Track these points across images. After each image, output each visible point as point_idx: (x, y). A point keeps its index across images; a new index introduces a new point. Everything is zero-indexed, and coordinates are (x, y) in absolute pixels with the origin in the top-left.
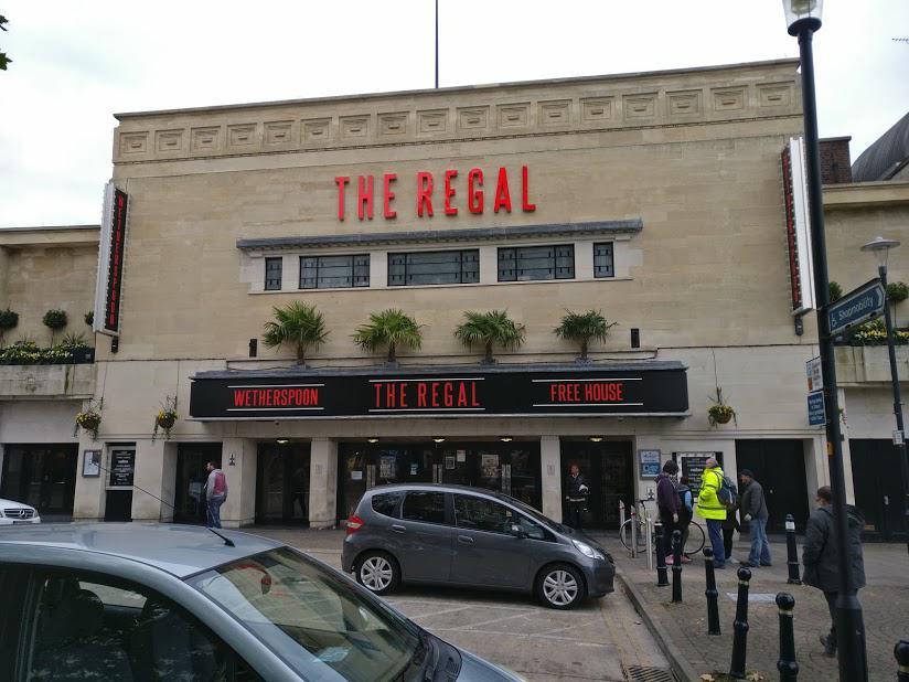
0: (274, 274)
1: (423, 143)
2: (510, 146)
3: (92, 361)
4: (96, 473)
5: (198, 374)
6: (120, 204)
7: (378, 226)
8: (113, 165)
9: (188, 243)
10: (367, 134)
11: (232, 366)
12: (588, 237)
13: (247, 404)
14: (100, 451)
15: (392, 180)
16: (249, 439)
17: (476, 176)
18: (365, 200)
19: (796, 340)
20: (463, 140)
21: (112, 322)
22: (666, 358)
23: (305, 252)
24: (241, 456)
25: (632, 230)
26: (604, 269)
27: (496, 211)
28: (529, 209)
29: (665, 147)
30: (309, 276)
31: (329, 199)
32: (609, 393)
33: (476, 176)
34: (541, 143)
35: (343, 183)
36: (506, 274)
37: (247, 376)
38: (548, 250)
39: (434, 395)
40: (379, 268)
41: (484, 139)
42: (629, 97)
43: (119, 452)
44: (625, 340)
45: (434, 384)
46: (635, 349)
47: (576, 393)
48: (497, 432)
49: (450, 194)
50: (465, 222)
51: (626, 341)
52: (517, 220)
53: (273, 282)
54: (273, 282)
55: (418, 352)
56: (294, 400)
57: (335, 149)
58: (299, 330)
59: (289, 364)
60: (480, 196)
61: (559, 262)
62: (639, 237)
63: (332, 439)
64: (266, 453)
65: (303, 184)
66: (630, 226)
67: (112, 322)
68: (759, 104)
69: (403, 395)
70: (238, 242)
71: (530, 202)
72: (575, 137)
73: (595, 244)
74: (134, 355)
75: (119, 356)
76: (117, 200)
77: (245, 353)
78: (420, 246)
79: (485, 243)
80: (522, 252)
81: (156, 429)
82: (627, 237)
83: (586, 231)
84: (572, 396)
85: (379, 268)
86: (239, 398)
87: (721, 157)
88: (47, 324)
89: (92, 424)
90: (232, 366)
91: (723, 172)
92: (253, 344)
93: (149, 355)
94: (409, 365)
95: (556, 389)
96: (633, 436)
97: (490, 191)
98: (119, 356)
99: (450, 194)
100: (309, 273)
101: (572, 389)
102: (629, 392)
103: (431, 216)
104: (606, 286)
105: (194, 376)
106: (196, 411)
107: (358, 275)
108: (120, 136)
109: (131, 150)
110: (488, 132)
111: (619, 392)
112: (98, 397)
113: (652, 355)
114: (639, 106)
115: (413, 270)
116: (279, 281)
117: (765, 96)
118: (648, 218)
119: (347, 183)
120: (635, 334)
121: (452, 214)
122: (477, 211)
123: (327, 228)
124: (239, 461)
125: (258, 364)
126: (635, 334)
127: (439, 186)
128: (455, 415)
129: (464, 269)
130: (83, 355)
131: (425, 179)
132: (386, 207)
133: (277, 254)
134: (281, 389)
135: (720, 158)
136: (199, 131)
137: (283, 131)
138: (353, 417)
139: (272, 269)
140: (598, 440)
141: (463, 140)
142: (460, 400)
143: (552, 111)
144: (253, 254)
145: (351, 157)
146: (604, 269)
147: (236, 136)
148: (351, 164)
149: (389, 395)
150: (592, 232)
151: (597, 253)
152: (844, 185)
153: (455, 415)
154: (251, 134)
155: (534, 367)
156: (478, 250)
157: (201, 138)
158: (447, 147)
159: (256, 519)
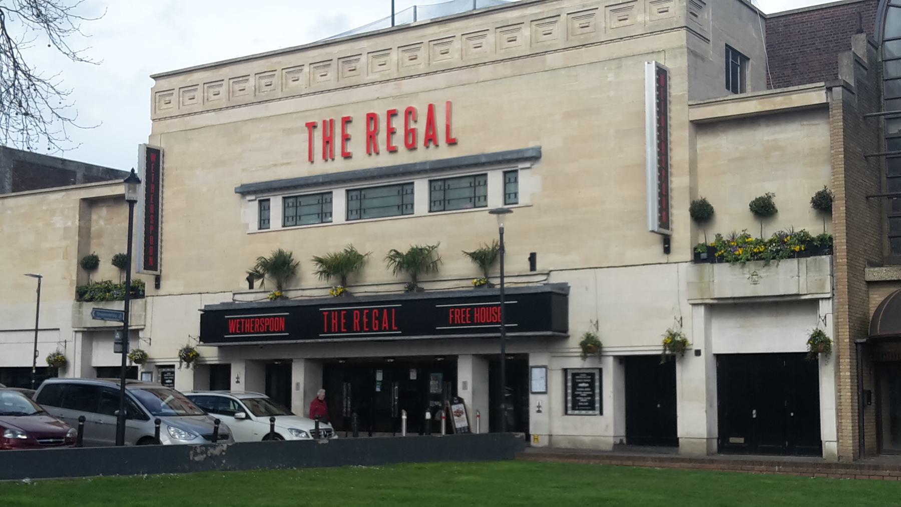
0: (511, 189)
1: (373, 83)
2: (440, 80)
3: (143, 296)
5: (205, 306)
6: (153, 157)
7: (338, 166)
8: (151, 122)
11: (237, 297)
12: (425, 176)
15: (347, 121)
17: (410, 112)
18: (328, 142)
19: (664, 258)
20: (404, 78)
22: (556, 279)
23: (351, 186)
24: (244, 374)
25: (534, 157)
28: (452, 142)
29: (563, 72)
33: (410, 112)
34: (464, 75)
35: (312, 126)
36: (356, 212)
37: (451, 296)
40: (339, 201)
41: (419, 75)
43: (166, 373)
49: (391, 132)
50: (404, 158)
51: (526, 265)
52: (443, 153)
56: (268, 326)
57: (308, 94)
59: (328, 291)
65: (284, 130)
66: (413, 169)
68: (648, 19)
69: (343, 321)
70: (236, 189)
72: (491, 66)
74: (172, 291)
75: (162, 291)
76: (148, 158)
82: (527, 165)
85: (339, 201)
86: (232, 328)
87: (611, 77)
88: (115, 265)
89: (591, 326)
90: (237, 297)
91: (612, 93)
93: (181, 290)
95: (453, 313)
96: (291, 360)
97: (421, 127)
99: (391, 132)
102: (511, 314)
103: (378, 153)
105: (203, 308)
108: (159, 96)
110: (422, 68)
113: (544, 277)
114: (546, 29)
117: (655, 9)
118: (549, 145)
119: (315, 127)
120: (533, 258)
121: (392, 150)
122: (411, 147)
123: (300, 169)
124: (242, 380)
125: (254, 295)
126: (533, 258)
128: (391, 338)
132: (343, 147)
133: (265, 196)
134: (259, 318)
135: (609, 79)
136: (469, 36)
139: (509, 182)
140: (392, 360)
141: (404, 78)
142: (384, 325)
143: (582, 22)
144: (249, 198)
149: (476, 315)
150: (499, 162)
152: (796, 88)
153: (391, 338)
154: (246, 85)
157: (212, 91)
158: (391, 84)
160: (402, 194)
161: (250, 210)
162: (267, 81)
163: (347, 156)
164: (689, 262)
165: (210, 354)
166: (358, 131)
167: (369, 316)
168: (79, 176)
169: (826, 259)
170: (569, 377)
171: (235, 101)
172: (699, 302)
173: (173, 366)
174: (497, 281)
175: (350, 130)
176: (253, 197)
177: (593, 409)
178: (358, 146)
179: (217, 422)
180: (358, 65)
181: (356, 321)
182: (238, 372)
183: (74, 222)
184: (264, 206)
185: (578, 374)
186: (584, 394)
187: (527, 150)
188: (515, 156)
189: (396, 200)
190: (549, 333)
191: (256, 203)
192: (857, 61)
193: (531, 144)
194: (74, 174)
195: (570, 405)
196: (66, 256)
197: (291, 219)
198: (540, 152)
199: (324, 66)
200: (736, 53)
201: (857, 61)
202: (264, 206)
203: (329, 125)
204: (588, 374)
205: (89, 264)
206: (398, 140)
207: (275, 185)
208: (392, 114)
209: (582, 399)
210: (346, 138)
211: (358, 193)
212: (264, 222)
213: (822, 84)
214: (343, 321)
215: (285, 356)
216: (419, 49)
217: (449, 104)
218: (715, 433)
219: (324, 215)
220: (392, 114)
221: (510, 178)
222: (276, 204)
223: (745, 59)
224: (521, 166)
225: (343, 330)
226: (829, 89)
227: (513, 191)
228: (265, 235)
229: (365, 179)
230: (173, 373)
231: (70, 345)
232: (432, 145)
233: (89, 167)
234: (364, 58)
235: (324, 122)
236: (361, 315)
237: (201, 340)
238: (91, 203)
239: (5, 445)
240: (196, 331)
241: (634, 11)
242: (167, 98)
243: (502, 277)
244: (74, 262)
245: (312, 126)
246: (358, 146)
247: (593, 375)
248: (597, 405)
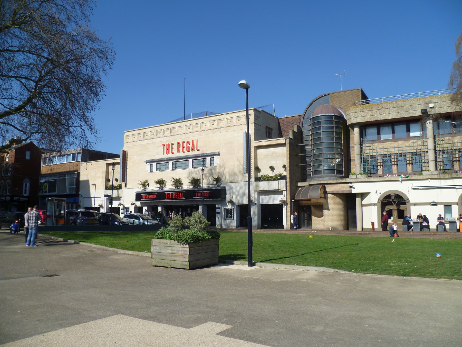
4: (259, 151)
7: (170, 156)
9: (137, 161)
15: (172, 144)
17: (188, 142)
28: (198, 150)
33: (188, 142)
35: (164, 145)
39: (176, 195)
49: (183, 147)
50: (186, 154)
52: (196, 153)
66: (187, 157)
69: (171, 196)
82: (216, 156)
86: (143, 197)
97: (190, 146)
99: (183, 147)
109: (127, 139)
115: (177, 165)
119: (165, 145)
123: (161, 156)
130: (120, 187)
145: (165, 139)
155: (110, 233)
160: (186, 163)
161: (148, 166)
162: (153, 133)
163: (173, 153)
164: (113, 184)
165: (139, 204)
166: (175, 147)
167: (177, 194)
168: (107, 156)
169: (285, 181)
170: (226, 210)
171: (145, 138)
172: (256, 191)
173: (129, 207)
174: (202, 186)
175: (173, 146)
176: (149, 163)
177: (232, 218)
178: (175, 150)
179: (134, 221)
180: (175, 130)
181: (174, 196)
182: (145, 208)
183: (104, 169)
184: (151, 166)
185: (228, 209)
186: (230, 214)
187: (216, 152)
188: (213, 154)
189: (184, 165)
190: (220, 199)
191: (150, 165)
192: (294, 132)
193: (217, 151)
194: (105, 156)
195: (226, 217)
196: (102, 178)
197: (158, 169)
198: (219, 153)
199: (167, 130)
200: (269, 128)
201: (294, 132)
202: (151, 166)
203: (168, 145)
204: (230, 209)
205: (108, 180)
206: (185, 149)
207: (155, 160)
208: (184, 143)
210: (172, 149)
211: (195, 160)
212: (151, 170)
213: (284, 138)
214: (171, 196)
215: (156, 205)
216: (190, 126)
217: (197, 140)
218: (260, 223)
219: (167, 169)
220: (184, 143)
221: (212, 160)
222: (155, 164)
223: (272, 129)
224: (214, 156)
226: (286, 139)
227: (205, 163)
228: (152, 173)
229: (177, 159)
230: (129, 209)
231: (103, 201)
232: (193, 151)
233: (109, 154)
234: (177, 128)
235: (167, 144)
236: (175, 194)
237: (136, 200)
238: (108, 165)
239: (366, 327)
240: (135, 198)
241: (242, 118)
242: (128, 137)
243: (203, 185)
244: (105, 180)
245: (164, 145)
246: (175, 150)
247: (232, 209)
248: (233, 217)
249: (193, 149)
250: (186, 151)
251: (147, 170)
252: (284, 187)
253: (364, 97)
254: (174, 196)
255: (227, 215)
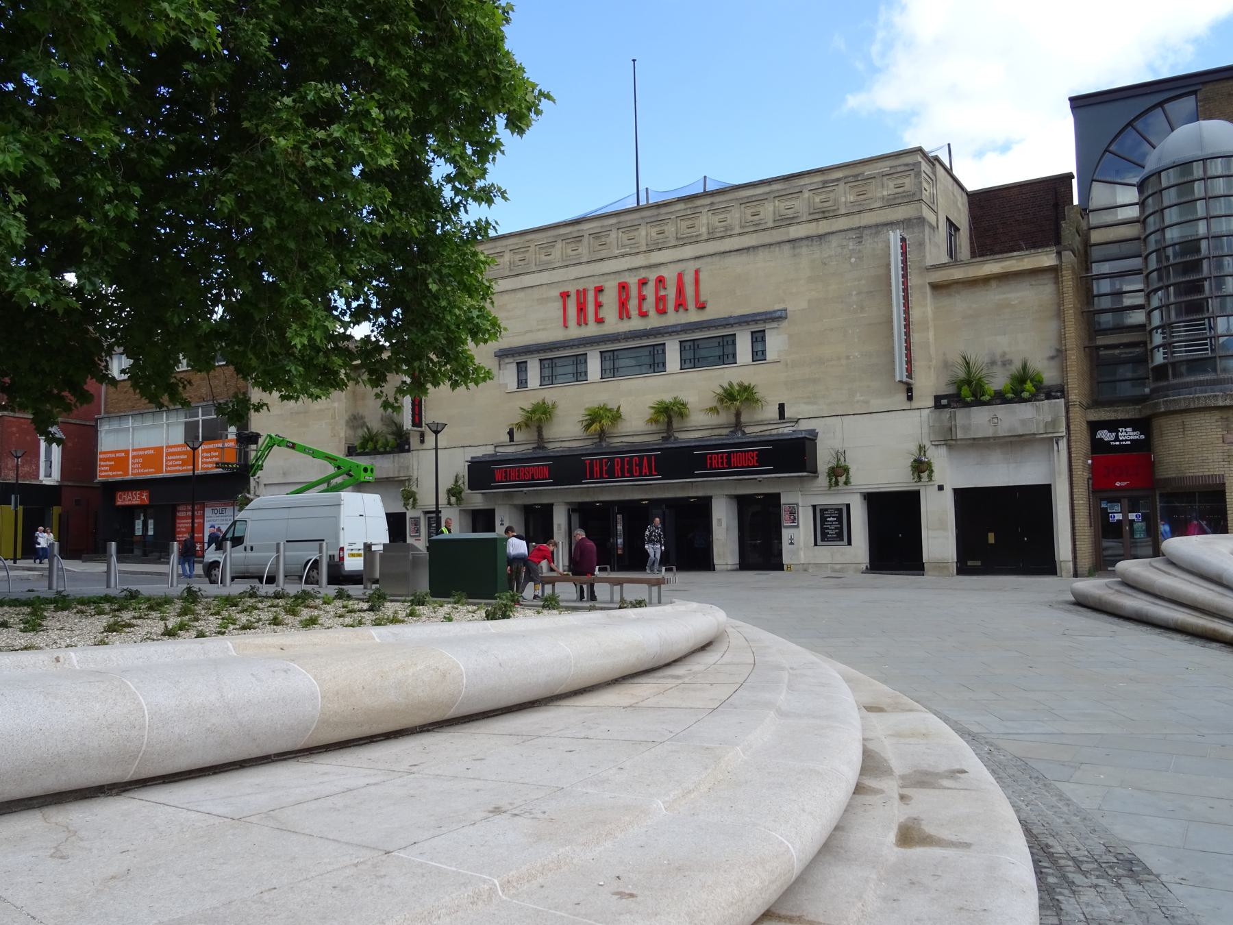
5: (472, 458)
7: (592, 330)
10: (584, 250)
11: (498, 449)
13: (504, 480)
14: (419, 518)
16: (515, 506)
19: (907, 405)
21: (417, 421)
22: (804, 426)
23: (543, 356)
25: (776, 317)
26: (759, 355)
27: (676, 309)
30: (608, 362)
31: (555, 309)
32: (749, 459)
35: (565, 295)
38: (718, 340)
39: (627, 467)
40: (594, 365)
42: (565, 239)
44: (773, 413)
45: (626, 459)
46: (781, 421)
47: (725, 460)
48: (637, 496)
49: (642, 298)
50: (654, 321)
52: (693, 316)
53: (522, 383)
54: (522, 383)
55: (689, 425)
56: (533, 474)
58: (539, 417)
59: (589, 442)
60: (663, 298)
61: (724, 353)
62: (785, 324)
63: (515, 506)
64: (743, 503)
67: (417, 421)
71: (702, 299)
73: (752, 333)
77: (506, 438)
78: (566, 352)
79: (740, 328)
80: (699, 342)
81: (449, 500)
83: (743, 321)
84: (722, 464)
85: (594, 365)
86: (498, 475)
90: (498, 449)
92: (511, 433)
94: (617, 442)
95: (711, 458)
97: (671, 293)
98: (915, 404)
99: (642, 298)
100: (547, 372)
101: (722, 458)
104: (761, 368)
105: (469, 459)
106: (472, 486)
107: (655, 363)
111: (756, 458)
112: (415, 477)
116: (764, 352)
118: (794, 305)
119: (568, 296)
120: (782, 407)
121: (643, 315)
122: (662, 311)
123: (556, 334)
125: (515, 447)
126: (782, 407)
127: (634, 292)
129: (655, 363)
131: (624, 287)
133: (522, 359)
134: (524, 467)
137: (828, 196)
138: (559, 487)
142: (644, 471)
144: (507, 360)
146: (759, 355)
147: (518, 257)
148: (571, 277)
151: (754, 340)
155: (699, 441)
156: (735, 334)
159: (740, 564)
166: (610, 299)
176: (511, 360)
184: (522, 368)
185: (826, 510)
202: (522, 368)
203: (582, 294)
209: (830, 532)
210: (598, 305)
221: (758, 338)
225: (654, 473)
235: (578, 291)
245: (565, 295)
249: (680, 304)
250: (652, 313)
251: (506, 385)
252: (1054, 422)
253: (282, 649)
254: (617, 468)
255: (841, 522)
